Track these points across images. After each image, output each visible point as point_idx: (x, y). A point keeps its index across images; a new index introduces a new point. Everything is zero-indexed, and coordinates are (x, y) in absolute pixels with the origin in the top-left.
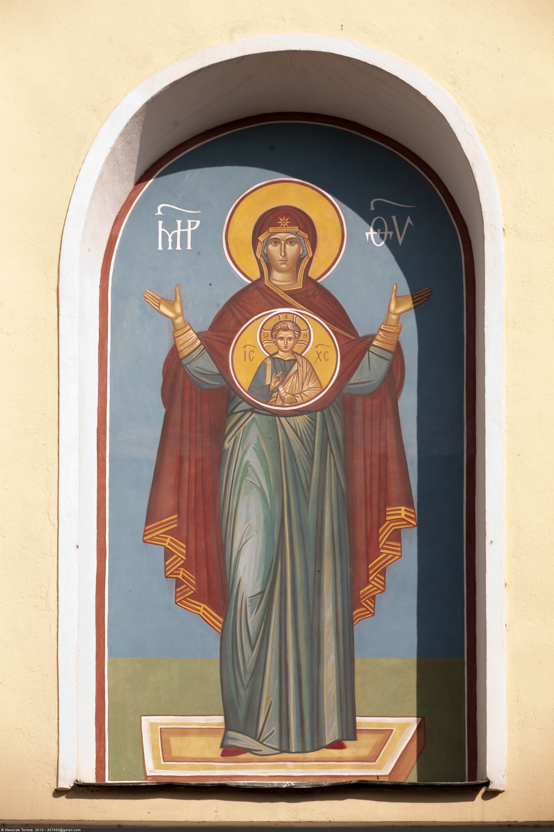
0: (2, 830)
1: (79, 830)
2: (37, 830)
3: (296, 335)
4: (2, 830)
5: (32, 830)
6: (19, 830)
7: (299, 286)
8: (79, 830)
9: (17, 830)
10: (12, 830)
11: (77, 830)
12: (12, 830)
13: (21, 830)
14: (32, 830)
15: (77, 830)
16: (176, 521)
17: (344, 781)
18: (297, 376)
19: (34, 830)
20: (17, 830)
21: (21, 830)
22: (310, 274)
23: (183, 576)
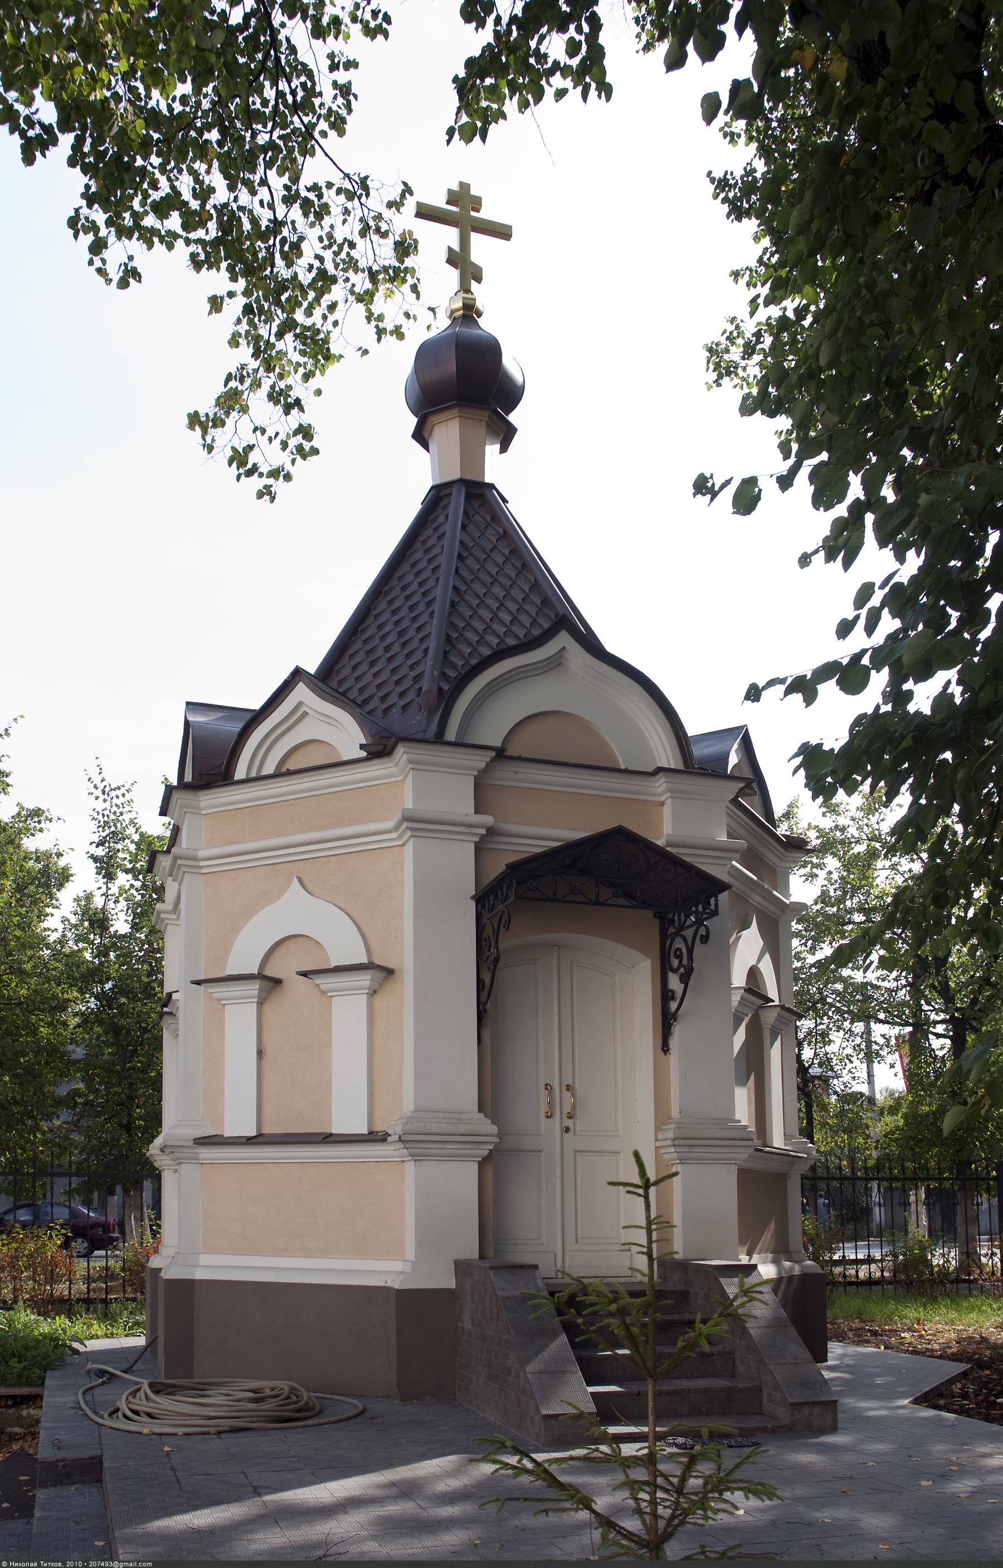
0: (4, 1564)
1: (150, 1564)
2: (69, 1564)
3: (644, 1505)
4: (4, 1564)
5: (60, 1564)
6: (36, 1565)
7: (183, 869)
8: (150, 1564)
9: (32, 1565)
10: (24, 1565)
11: (144, 1565)
12: (24, 1565)
13: (39, 1564)
14: (60, 1564)
15: (144, 1565)
16: (96, 1194)
17: (926, 1390)
18: (756, 1292)
19: (64, 1564)
20: (32, 1565)
21: (39, 1564)
22: (266, 188)
23: (475, 225)
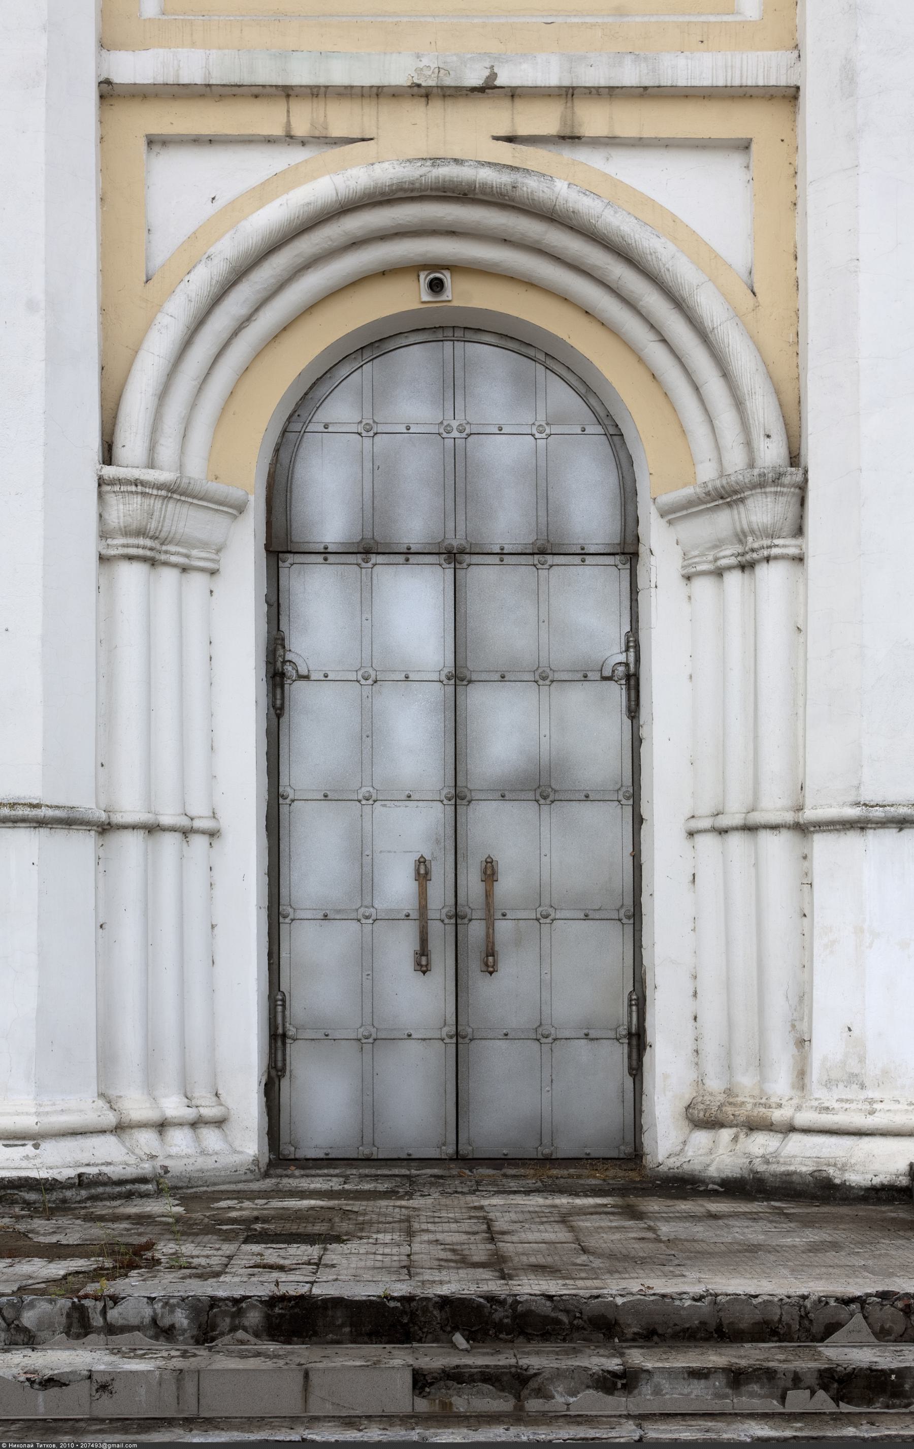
5: (54, 1446)
6: (32, 1446)
10: (21, 1446)
14: (54, 1446)
20: (29, 1446)
